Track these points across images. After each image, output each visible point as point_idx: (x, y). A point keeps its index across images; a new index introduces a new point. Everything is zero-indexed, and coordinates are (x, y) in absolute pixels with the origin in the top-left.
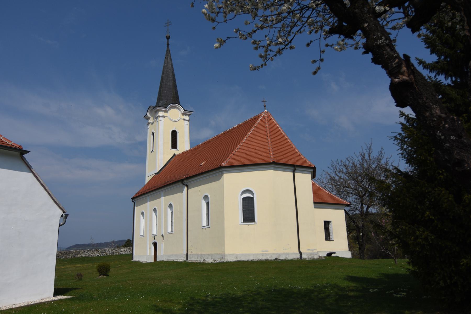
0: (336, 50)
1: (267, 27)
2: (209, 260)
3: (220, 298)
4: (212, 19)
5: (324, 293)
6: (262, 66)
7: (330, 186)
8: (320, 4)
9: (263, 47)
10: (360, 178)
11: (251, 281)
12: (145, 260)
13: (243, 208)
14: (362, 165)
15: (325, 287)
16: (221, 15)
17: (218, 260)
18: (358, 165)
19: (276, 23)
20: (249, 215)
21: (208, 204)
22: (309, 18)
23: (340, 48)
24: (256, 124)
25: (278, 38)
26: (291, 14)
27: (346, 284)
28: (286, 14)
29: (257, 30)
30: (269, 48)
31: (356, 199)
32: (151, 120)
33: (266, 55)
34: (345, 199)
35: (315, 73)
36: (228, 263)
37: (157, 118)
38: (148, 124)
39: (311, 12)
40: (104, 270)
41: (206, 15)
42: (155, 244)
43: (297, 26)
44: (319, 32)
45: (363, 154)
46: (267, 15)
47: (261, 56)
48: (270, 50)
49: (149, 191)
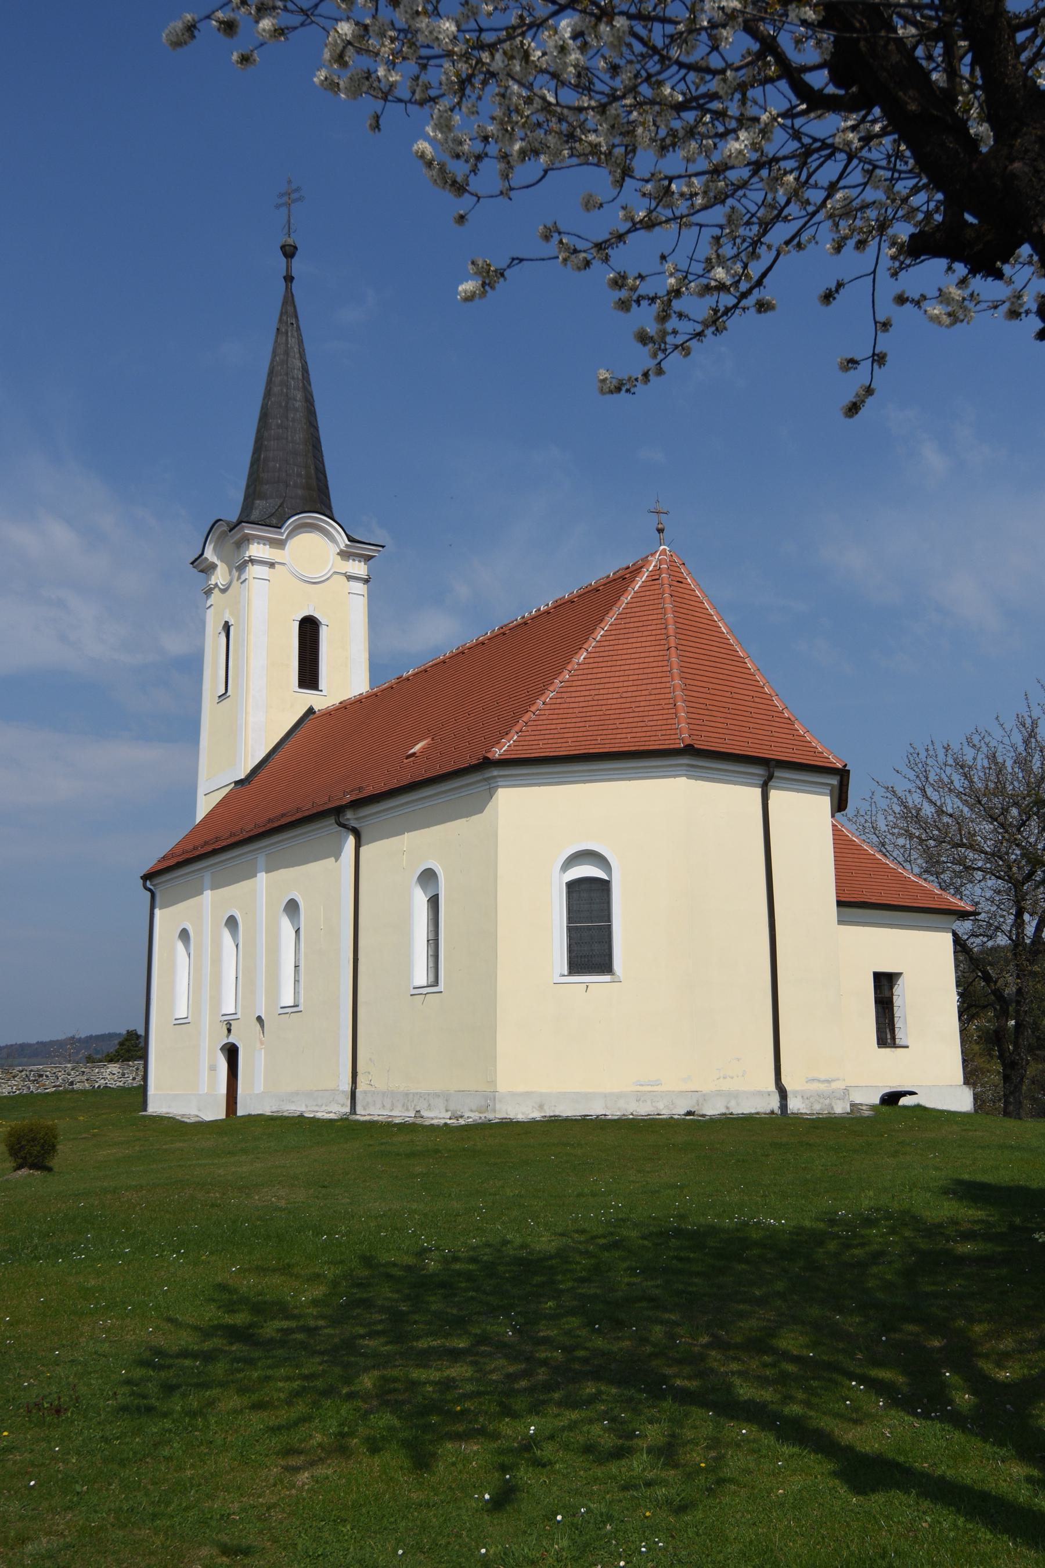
0: (935, 319)
1: (667, 221)
2: (437, 1115)
3: (473, 1260)
4: (454, 182)
5: (862, 1245)
6: (646, 375)
7: (901, 841)
8: (878, 136)
9: (653, 300)
10: (1014, 812)
11: (594, 1195)
12: (193, 1111)
13: (570, 920)
14: (1023, 763)
15: (869, 1222)
16: (491, 168)
17: (472, 1116)
18: (1009, 763)
19: (705, 208)
20: (590, 948)
21: (434, 902)
22: (832, 188)
23: (949, 315)
24: (627, 598)
25: (709, 265)
26: (764, 173)
27: (948, 1210)
28: (745, 173)
29: (629, 231)
30: (677, 305)
31: (999, 892)
32: (220, 576)
33: (664, 334)
34: (958, 891)
35: (853, 409)
36: (508, 1125)
37: (241, 568)
38: (208, 592)
39: (840, 166)
40: (33, 1150)
41: (429, 164)
42: (231, 1053)
43: (786, 219)
44: (873, 244)
45: (1028, 722)
46: (670, 174)
47: (643, 338)
48: (680, 315)
49: (209, 848)
